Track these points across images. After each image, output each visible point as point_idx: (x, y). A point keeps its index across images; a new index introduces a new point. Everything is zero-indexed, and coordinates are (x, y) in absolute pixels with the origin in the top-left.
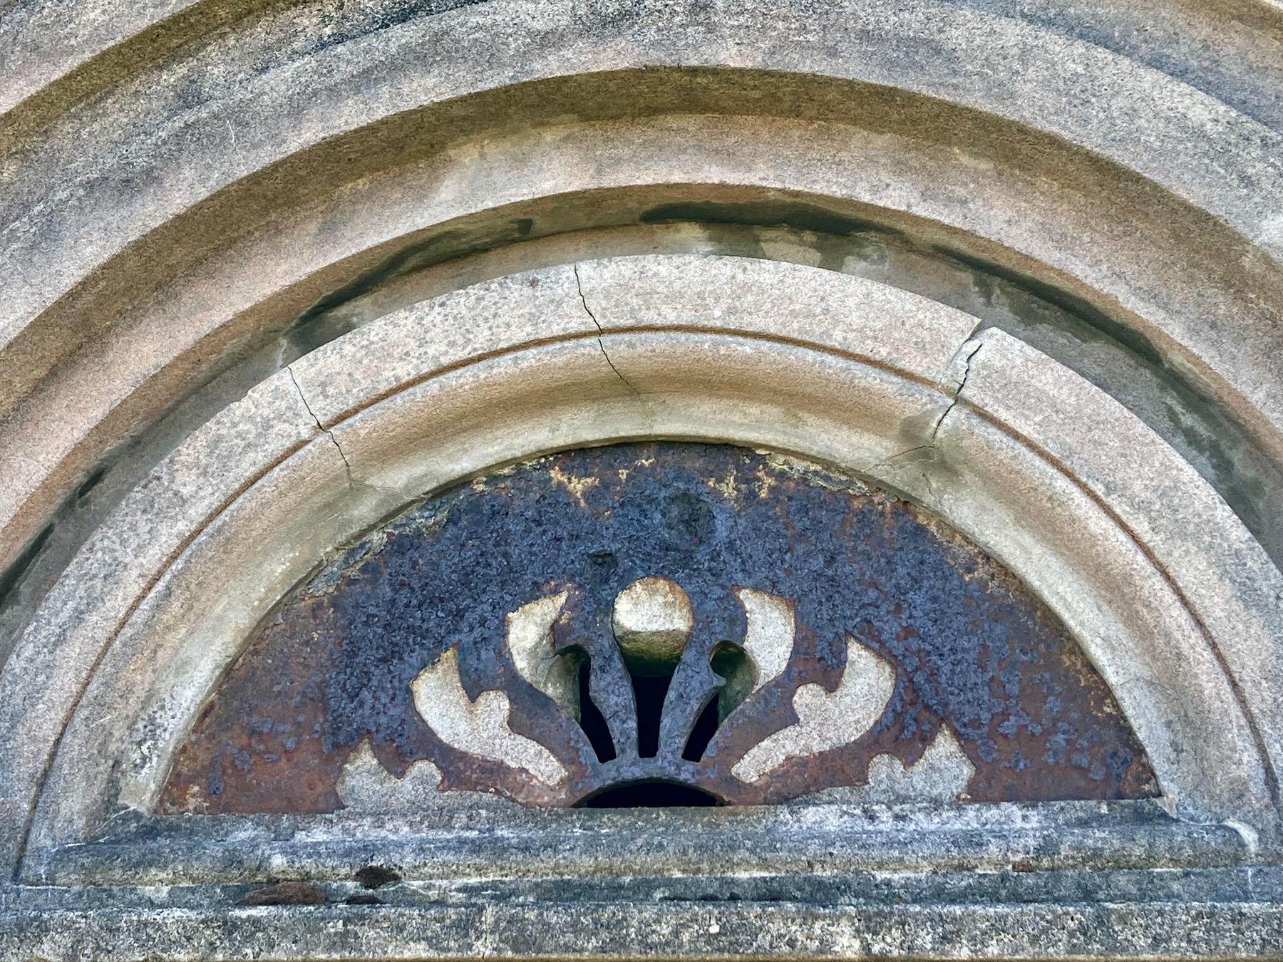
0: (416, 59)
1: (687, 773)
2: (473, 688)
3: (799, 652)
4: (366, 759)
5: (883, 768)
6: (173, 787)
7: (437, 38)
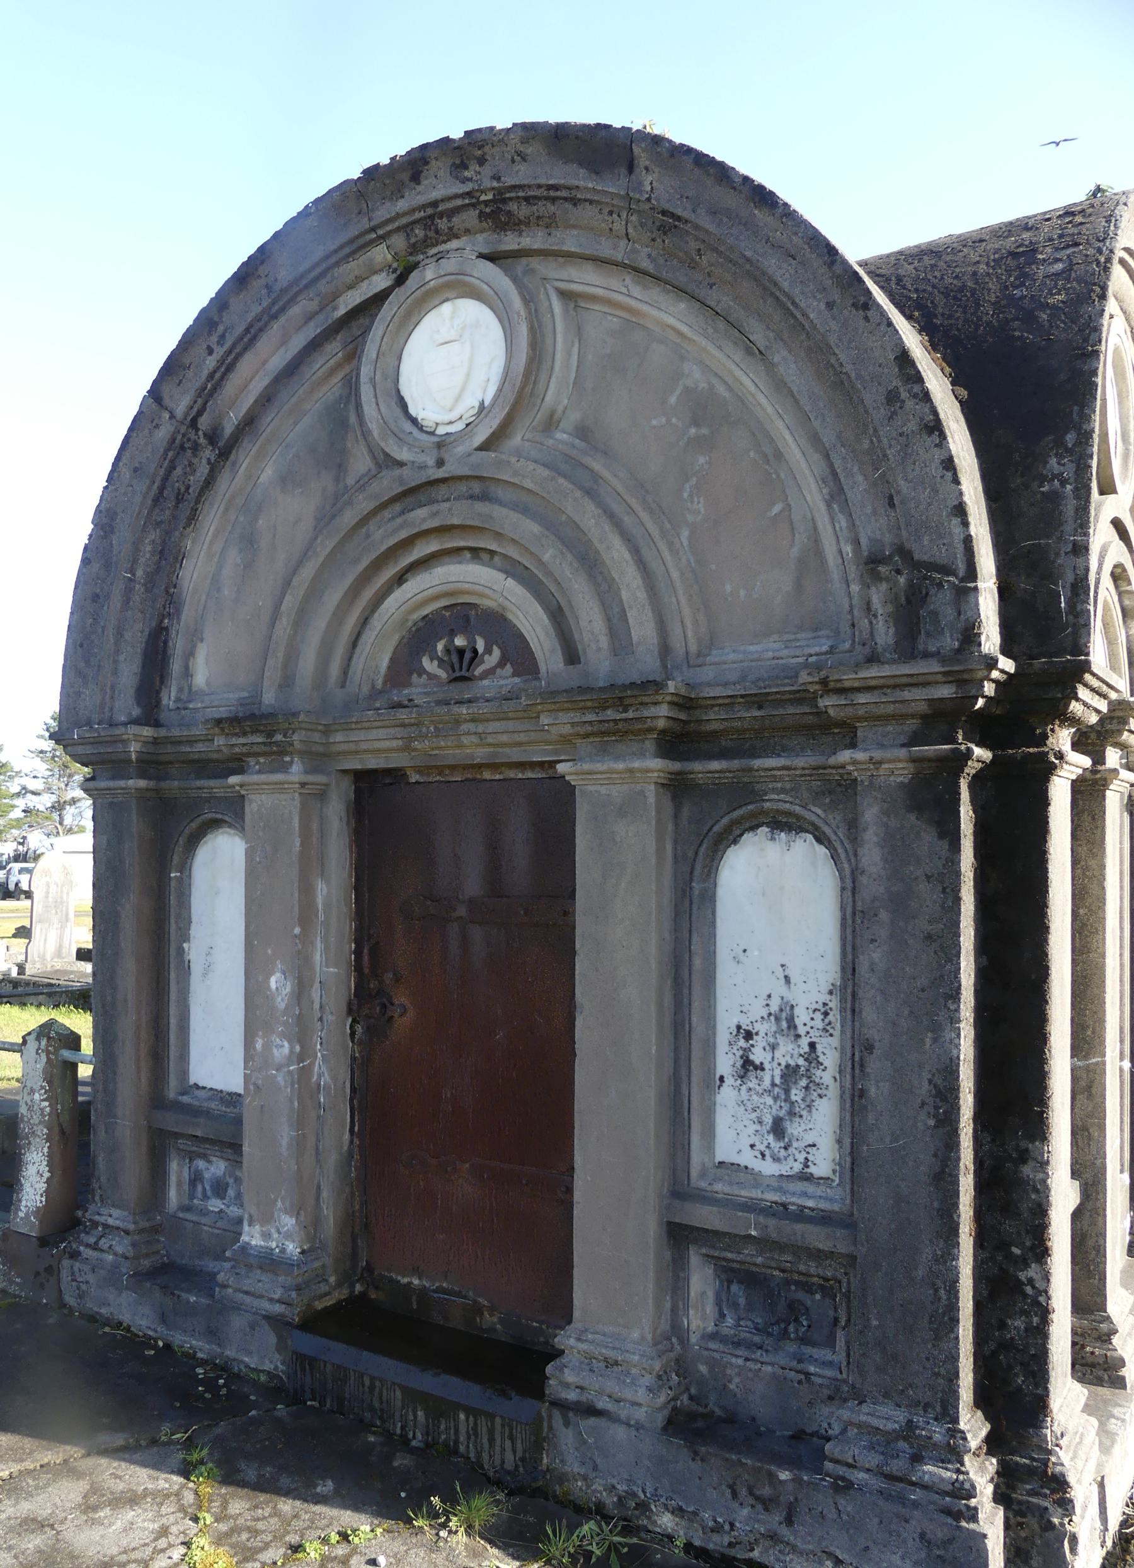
0: (402, 527)
1: (467, 674)
2: (432, 660)
3: (485, 648)
4: (415, 675)
5: (499, 671)
6: (385, 683)
7: (405, 521)
